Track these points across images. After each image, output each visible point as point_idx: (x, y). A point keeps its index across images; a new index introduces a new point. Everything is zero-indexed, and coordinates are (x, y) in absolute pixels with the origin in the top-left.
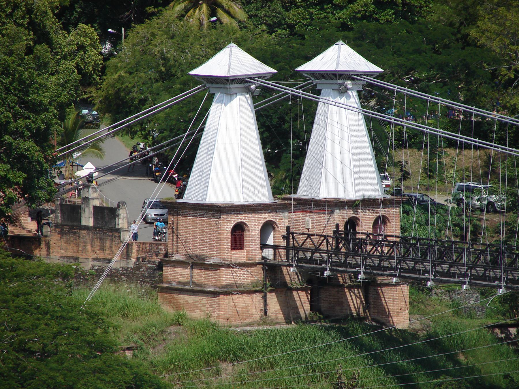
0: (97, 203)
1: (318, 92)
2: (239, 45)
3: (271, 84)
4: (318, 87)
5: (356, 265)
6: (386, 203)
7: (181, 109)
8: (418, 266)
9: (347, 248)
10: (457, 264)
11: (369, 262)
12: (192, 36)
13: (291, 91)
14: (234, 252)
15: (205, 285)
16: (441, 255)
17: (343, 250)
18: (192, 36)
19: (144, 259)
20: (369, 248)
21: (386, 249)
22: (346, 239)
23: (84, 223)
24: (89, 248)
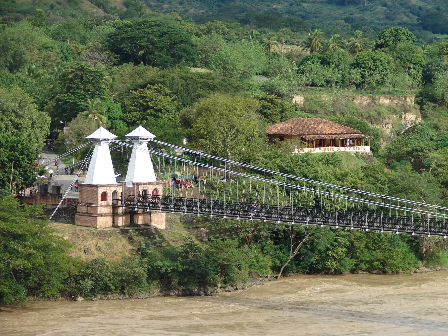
0: (53, 184)
1: (133, 144)
2: (144, 127)
3: (116, 142)
4: (133, 142)
5: (146, 206)
6: (157, 184)
7: (277, 156)
8: (219, 211)
9: (143, 200)
10: (170, 205)
11: (151, 205)
12: (283, 125)
13: (122, 144)
14: (103, 202)
15: (92, 214)
16: (202, 204)
17: (142, 201)
18: (283, 125)
19: (70, 204)
20: (151, 200)
21: (157, 200)
22: (143, 197)
23: (48, 191)
24: (50, 200)
